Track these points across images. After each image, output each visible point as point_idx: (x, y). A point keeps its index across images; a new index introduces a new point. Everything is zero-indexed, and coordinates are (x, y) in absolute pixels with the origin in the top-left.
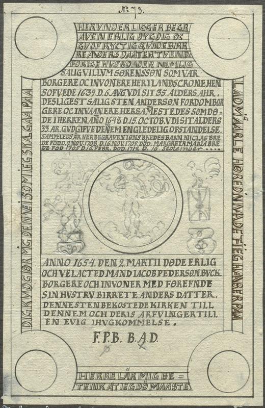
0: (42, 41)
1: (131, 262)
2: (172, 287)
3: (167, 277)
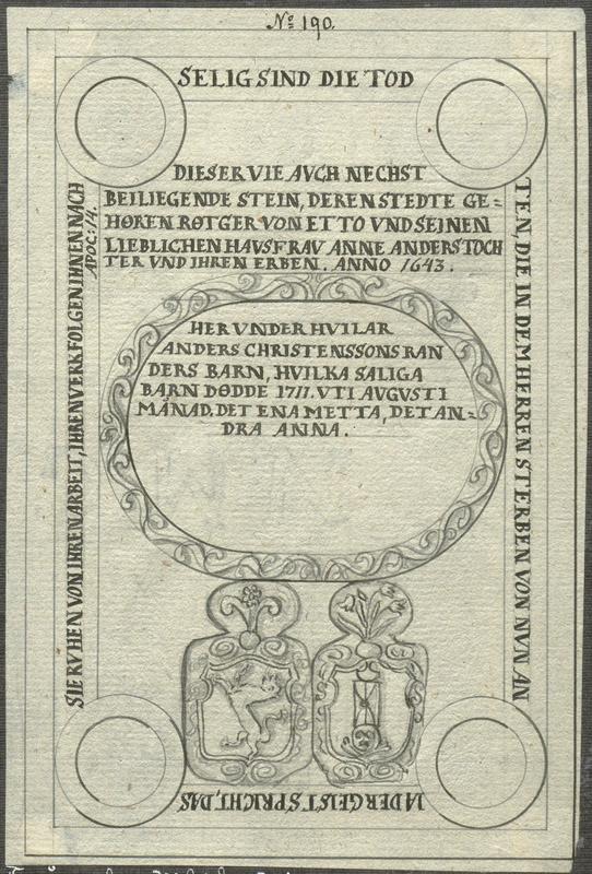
0: (486, 96)
1: (146, 408)
2: (94, 254)
3: (273, 209)
